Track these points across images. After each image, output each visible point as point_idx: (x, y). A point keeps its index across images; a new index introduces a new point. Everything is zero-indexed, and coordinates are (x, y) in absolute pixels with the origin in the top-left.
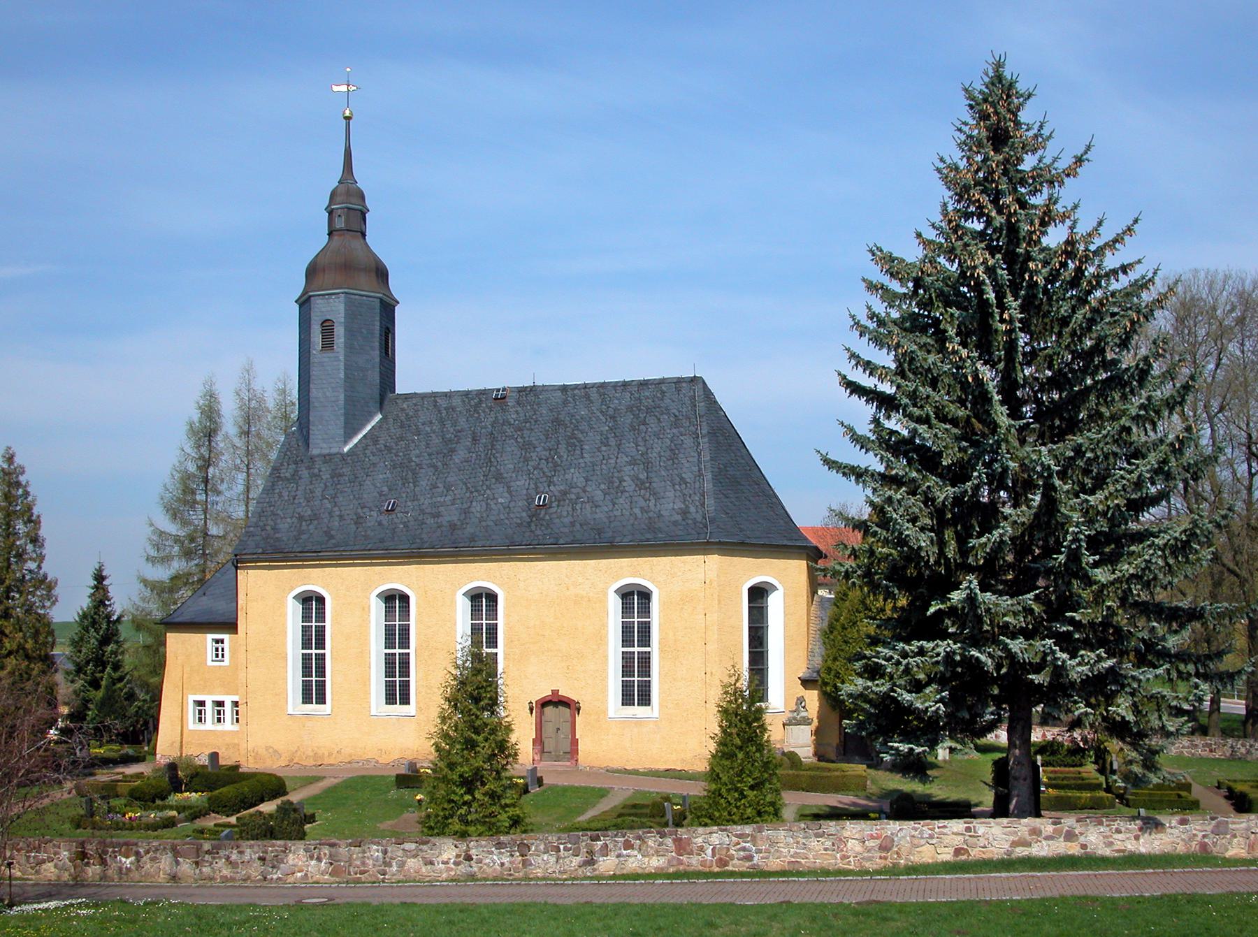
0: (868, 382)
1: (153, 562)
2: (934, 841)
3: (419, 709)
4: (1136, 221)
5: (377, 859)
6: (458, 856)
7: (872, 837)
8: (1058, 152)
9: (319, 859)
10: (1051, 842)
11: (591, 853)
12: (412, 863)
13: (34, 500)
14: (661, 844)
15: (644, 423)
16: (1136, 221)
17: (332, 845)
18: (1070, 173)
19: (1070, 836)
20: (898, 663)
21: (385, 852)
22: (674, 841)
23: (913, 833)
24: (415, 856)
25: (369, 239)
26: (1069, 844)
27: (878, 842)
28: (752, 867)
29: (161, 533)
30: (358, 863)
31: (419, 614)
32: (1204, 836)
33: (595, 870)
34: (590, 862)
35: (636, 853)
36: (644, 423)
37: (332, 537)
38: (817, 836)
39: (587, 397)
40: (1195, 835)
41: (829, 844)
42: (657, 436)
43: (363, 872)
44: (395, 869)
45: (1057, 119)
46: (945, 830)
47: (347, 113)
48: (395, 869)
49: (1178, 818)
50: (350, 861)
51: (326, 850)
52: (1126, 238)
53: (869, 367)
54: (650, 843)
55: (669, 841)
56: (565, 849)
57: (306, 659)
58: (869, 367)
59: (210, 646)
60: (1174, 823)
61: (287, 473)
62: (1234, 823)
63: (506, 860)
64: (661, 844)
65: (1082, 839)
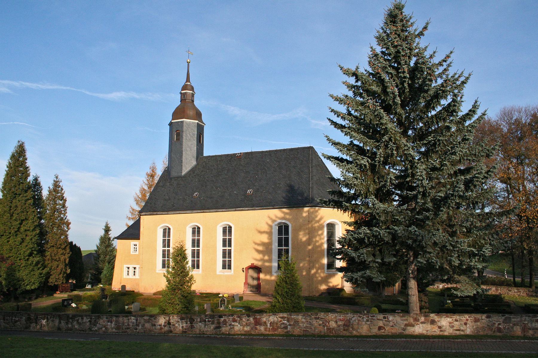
0: (339, 121)
1: (129, 219)
2: (369, 323)
3: (203, 270)
4: (451, 52)
5: (133, 323)
6: (165, 323)
7: (340, 320)
8: (417, 26)
9: (111, 322)
10: (424, 325)
11: (219, 323)
12: (148, 325)
13: (36, 179)
14: (248, 320)
15: (290, 163)
16: (451, 52)
17: (117, 317)
18: (421, 34)
19: (433, 322)
20: (466, 289)
21: (137, 320)
22: (254, 319)
23: (359, 318)
24: (149, 322)
25: (195, 103)
26: (433, 326)
27: (343, 322)
28: (287, 332)
29: (133, 210)
30: (126, 324)
31: (203, 235)
32: (499, 324)
33: (220, 331)
34: (218, 327)
35: (237, 324)
36: (290, 163)
37: (174, 206)
38: (316, 318)
39: (270, 155)
40: (494, 324)
41: (321, 322)
42: (294, 167)
43: (128, 328)
44: (140, 327)
45: (416, 16)
46: (374, 318)
47: (188, 61)
48: (140, 327)
49: (485, 315)
50: (123, 323)
51: (114, 319)
52: (424, 33)
53: (338, 114)
54: (244, 320)
55: (251, 319)
56: (209, 321)
57: (164, 251)
58: (338, 114)
59: (132, 247)
60: (483, 317)
61: (161, 184)
62: (514, 318)
63: (184, 325)
64: (248, 320)
65: (439, 324)
